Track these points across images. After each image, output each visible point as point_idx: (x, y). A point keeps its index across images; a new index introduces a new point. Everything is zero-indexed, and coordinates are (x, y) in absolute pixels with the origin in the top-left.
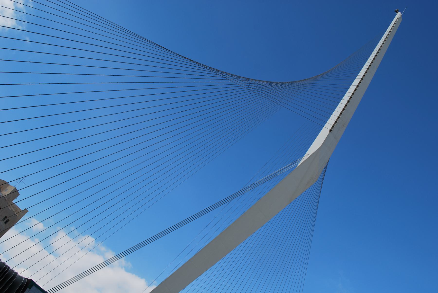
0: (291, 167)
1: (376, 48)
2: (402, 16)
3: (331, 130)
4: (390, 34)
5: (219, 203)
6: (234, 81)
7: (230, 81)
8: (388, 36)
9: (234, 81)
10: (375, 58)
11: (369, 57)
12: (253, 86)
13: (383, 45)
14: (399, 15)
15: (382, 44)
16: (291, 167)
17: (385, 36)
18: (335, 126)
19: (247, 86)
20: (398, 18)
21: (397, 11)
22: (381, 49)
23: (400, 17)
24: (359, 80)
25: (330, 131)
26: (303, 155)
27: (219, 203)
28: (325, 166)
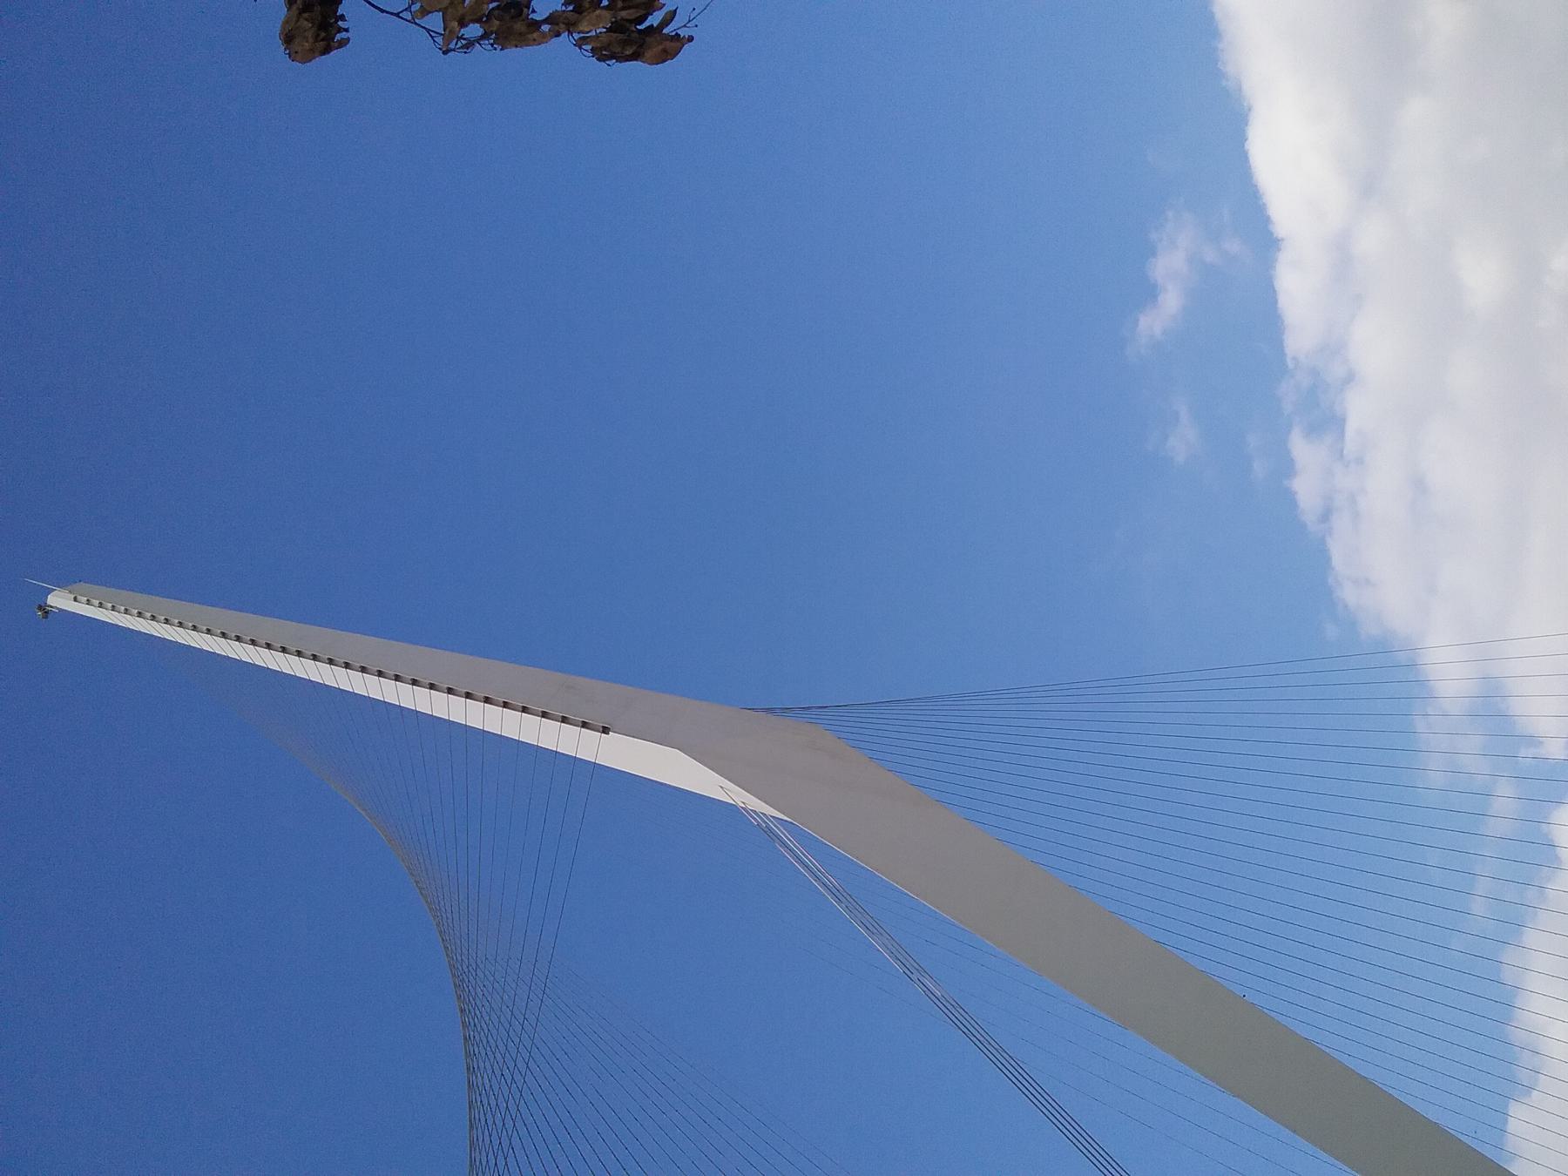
0: (790, 840)
1: (184, 642)
2: (63, 582)
3: (601, 729)
4: (278, 643)
5: (1095, 1146)
6: (501, 1163)
7: (511, 1160)
8: (149, 615)
9: (501, 1163)
10: (297, 651)
11: (255, 664)
12: (500, 1095)
13: (205, 628)
14: (59, 600)
15: (226, 638)
16: (790, 840)
17: (149, 627)
18: (541, 709)
19: (494, 1161)
20: (75, 599)
21: (45, 611)
22: (219, 631)
23: (70, 592)
24: (372, 680)
25: (605, 730)
26: (731, 809)
27: (1095, 1146)
28: (771, 717)
